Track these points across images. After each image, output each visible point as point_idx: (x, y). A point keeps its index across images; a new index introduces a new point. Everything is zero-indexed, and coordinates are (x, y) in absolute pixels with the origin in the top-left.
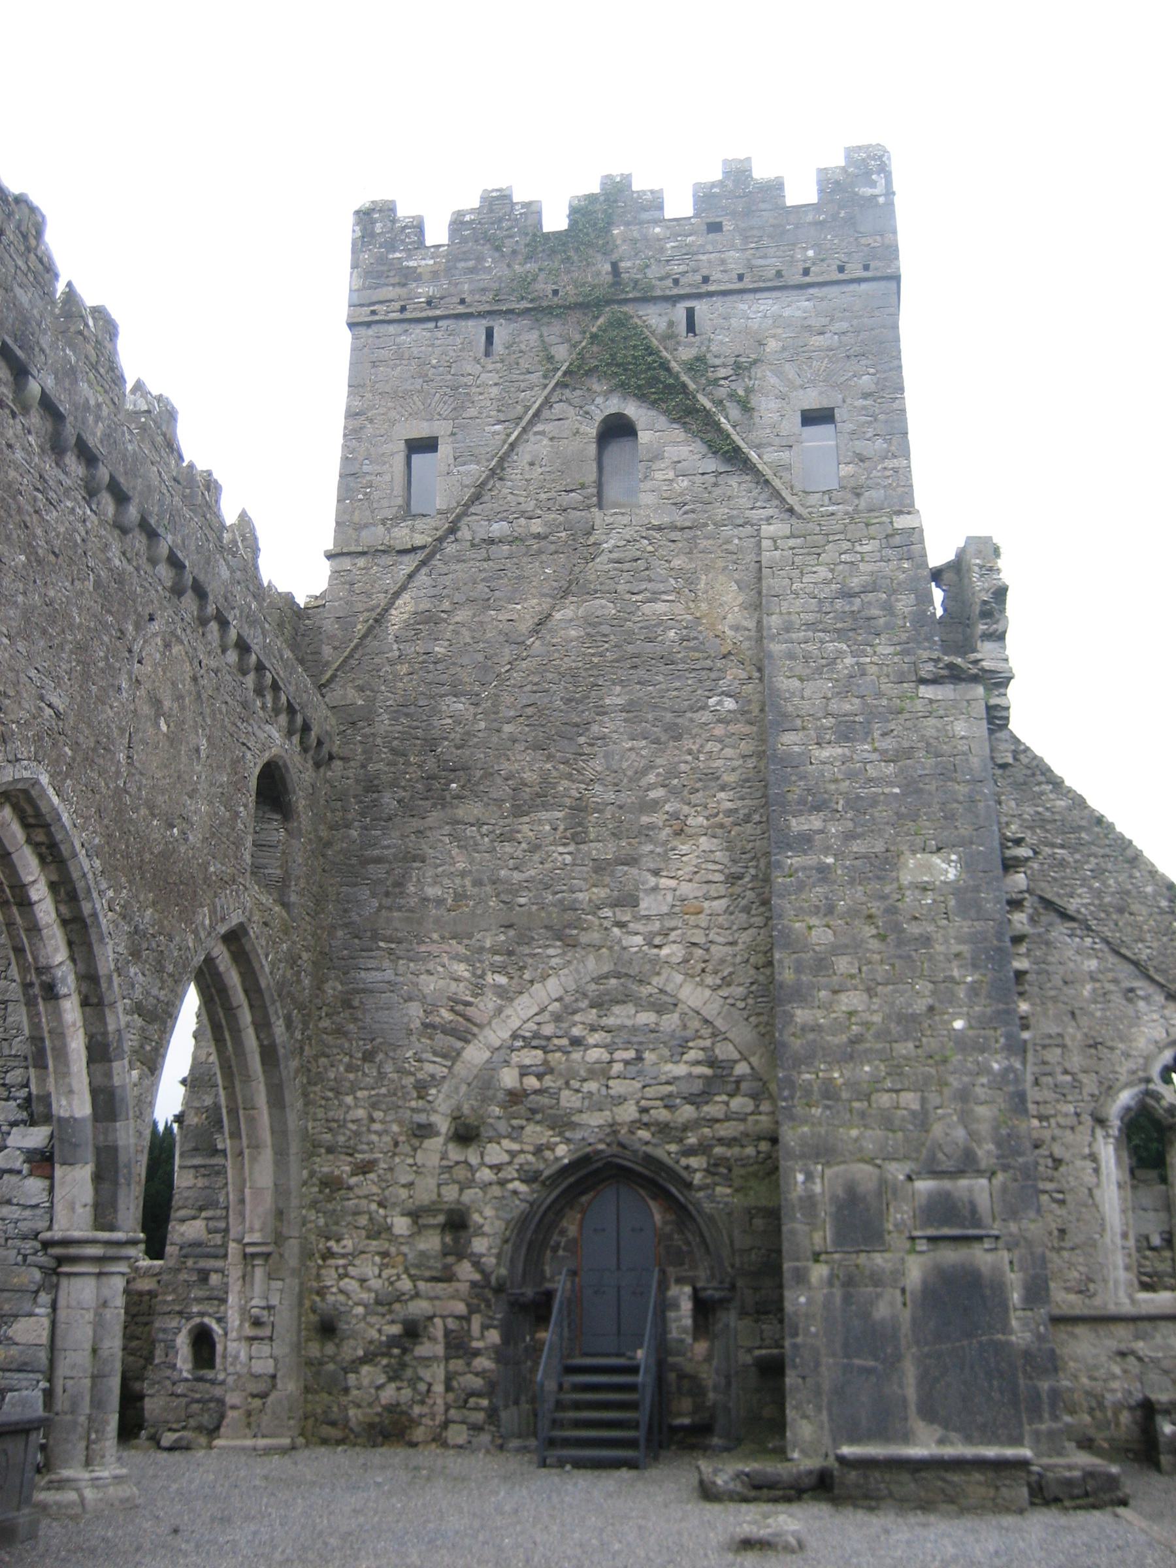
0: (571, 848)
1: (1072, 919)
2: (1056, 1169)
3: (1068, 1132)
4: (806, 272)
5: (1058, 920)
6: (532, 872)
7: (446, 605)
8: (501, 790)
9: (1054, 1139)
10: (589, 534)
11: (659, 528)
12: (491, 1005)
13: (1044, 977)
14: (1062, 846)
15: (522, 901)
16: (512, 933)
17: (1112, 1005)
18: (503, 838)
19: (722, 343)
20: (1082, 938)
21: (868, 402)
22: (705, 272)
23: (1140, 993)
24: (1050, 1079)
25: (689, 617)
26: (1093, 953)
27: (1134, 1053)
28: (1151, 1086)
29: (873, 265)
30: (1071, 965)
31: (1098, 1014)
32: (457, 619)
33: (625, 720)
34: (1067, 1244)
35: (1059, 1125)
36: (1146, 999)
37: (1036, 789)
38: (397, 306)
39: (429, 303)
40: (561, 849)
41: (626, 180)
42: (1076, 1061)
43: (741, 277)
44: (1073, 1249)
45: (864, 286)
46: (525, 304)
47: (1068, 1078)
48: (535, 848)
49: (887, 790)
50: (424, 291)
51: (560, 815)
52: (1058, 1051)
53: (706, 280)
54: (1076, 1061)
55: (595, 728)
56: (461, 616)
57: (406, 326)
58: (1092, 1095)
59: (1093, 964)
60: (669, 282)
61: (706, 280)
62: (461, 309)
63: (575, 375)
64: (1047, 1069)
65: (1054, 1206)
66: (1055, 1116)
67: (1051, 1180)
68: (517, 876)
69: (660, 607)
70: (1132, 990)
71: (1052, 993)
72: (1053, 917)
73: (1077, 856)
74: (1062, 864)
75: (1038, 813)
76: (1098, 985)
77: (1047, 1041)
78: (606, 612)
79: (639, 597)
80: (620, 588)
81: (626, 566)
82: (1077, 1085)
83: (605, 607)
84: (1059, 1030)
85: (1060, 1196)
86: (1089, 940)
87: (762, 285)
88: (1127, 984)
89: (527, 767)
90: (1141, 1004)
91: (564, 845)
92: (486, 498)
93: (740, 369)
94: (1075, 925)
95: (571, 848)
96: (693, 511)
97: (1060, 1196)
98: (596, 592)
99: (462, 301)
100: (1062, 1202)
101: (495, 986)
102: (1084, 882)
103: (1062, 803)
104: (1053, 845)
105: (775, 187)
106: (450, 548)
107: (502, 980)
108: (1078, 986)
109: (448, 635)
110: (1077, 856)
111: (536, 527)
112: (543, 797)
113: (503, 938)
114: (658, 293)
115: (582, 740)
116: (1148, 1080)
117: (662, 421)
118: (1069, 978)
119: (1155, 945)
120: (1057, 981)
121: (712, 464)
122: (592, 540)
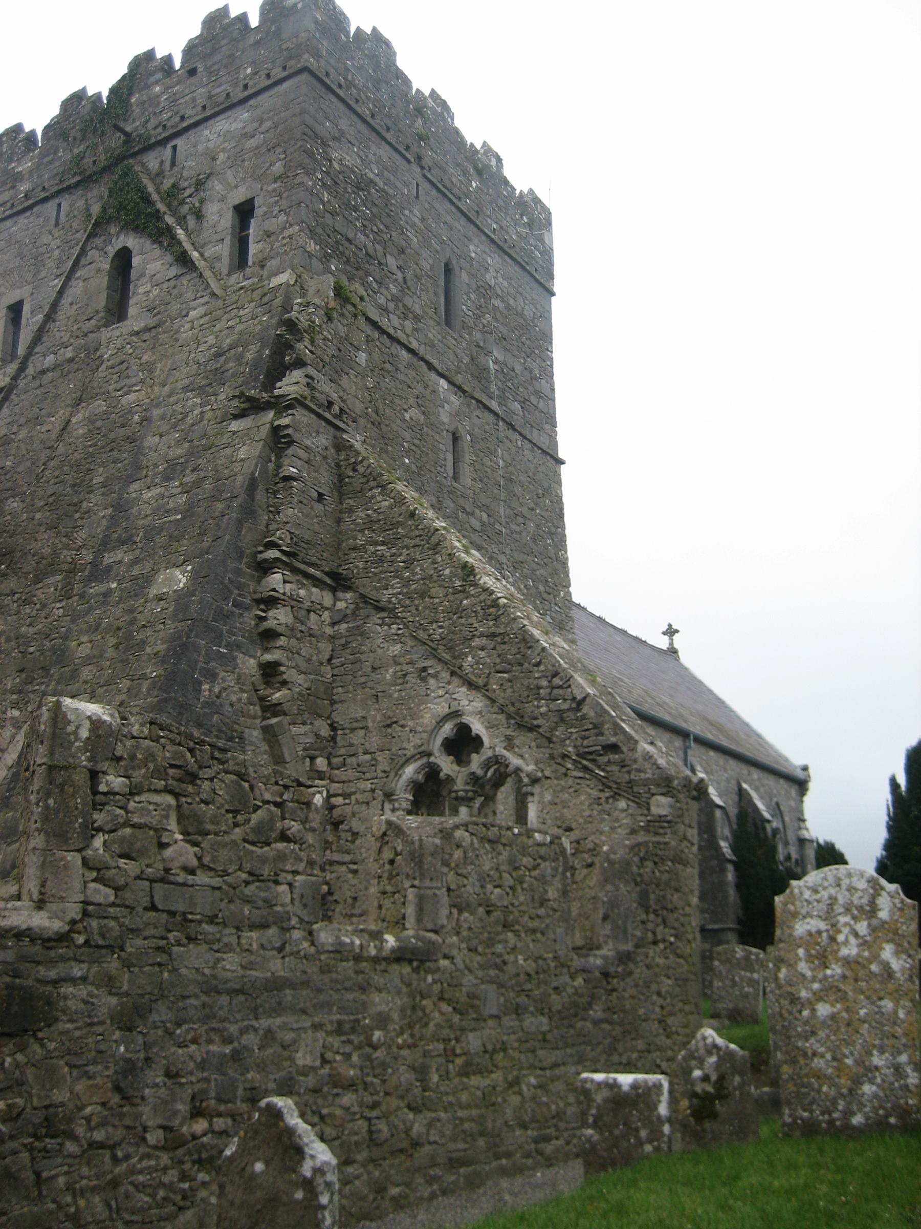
0: (63, 604)
1: (382, 609)
2: (353, 842)
3: (364, 807)
4: (246, 87)
5: (374, 612)
6: (40, 627)
7: (15, 429)
8: (29, 565)
9: (354, 815)
10: (97, 349)
11: (137, 333)
12: (9, 734)
13: (358, 665)
14: (383, 543)
15: (32, 649)
16: (24, 676)
17: (409, 685)
18: (26, 602)
19: (190, 168)
20: (389, 626)
21: (279, 184)
22: (181, 114)
23: (431, 671)
24: (354, 759)
25: (147, 401)
26: (398, 638)
27: (419, 729)
28: (432, 759)
29: (289, 64)
30: (380, 651)
31: (396, 695)
32: (20, 437)
33: (103, 494)
34: (357, 911)
35: (357, 802)
36: (435, 676)
37: (370, 494)
38: (9, 205)
39: (26, 196)
40: (58, 605)
41: (84, 90)
42: (374, 741)
43: (204, 107)
44: (361, 915)
45: (285, 85)
46: (78, 178)
47: (368, 757)
48: (44, 606)
49: (172, 518)
50: (24, 187)
51: (59, 578)
52: (361, 733)
53: (183, 118)
54: (374, 741)
55: (85, 504)
56: (23, 434)
57: (15, 219)
58: (385, 772)
59: (396, 649)
60: (160, 129)
61: (183, 118)
62: (43, 195)
63: (98, 227)
64: (352, 750)
65: (350, 875)
66: (355, 793)
67: (348, 852)
68: (32, 630)
69: (132, 397)
70: (424, 669)
71: (362, 680)
72: (370, 610)
73: (394, 551)
74: (381, 559)
75: (367, 515)
76: (398, 668)
77: (355, 725)
78: (101, 409)
79: (120, 393)
80: (111, 388)
81: (116, 370)
82: (374, 763)
83: (100, 405)
84: (362, 713)
85: (355, 867)
86: (395, 626)
87: (217, 109)
88: (421, 664)
89: (44, 543)
90: (432, 681)
91: (60, 601)
92: (44, 339)
93: (199, 184)
94: (385, 615)
95: (63, 604)
96: (159, 313)
97: (355, 867)
98: (97, 394)
99: (44, 189)
100: (355, 872)
101: (12, 718)
102: (397, 574)
103: (386, 503)
104: (376, 543)
105: (243, 18)
106: (21, 384)
107: (16, 713)
108: (382, 671)
109: (13, 452)
110: (394, 551)
111: (69, 353)
112: (51, 567)
113: (18, 680)
114: (153, 140)
115: (77, 516)
116: (430, 754)
117: (148, 244)
118: (376, 665)
119: (446, 624)
120: (367, 669)
121: (174, 271)
122: (98, 354)
